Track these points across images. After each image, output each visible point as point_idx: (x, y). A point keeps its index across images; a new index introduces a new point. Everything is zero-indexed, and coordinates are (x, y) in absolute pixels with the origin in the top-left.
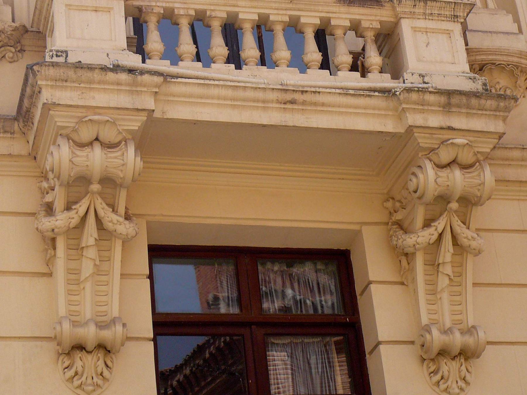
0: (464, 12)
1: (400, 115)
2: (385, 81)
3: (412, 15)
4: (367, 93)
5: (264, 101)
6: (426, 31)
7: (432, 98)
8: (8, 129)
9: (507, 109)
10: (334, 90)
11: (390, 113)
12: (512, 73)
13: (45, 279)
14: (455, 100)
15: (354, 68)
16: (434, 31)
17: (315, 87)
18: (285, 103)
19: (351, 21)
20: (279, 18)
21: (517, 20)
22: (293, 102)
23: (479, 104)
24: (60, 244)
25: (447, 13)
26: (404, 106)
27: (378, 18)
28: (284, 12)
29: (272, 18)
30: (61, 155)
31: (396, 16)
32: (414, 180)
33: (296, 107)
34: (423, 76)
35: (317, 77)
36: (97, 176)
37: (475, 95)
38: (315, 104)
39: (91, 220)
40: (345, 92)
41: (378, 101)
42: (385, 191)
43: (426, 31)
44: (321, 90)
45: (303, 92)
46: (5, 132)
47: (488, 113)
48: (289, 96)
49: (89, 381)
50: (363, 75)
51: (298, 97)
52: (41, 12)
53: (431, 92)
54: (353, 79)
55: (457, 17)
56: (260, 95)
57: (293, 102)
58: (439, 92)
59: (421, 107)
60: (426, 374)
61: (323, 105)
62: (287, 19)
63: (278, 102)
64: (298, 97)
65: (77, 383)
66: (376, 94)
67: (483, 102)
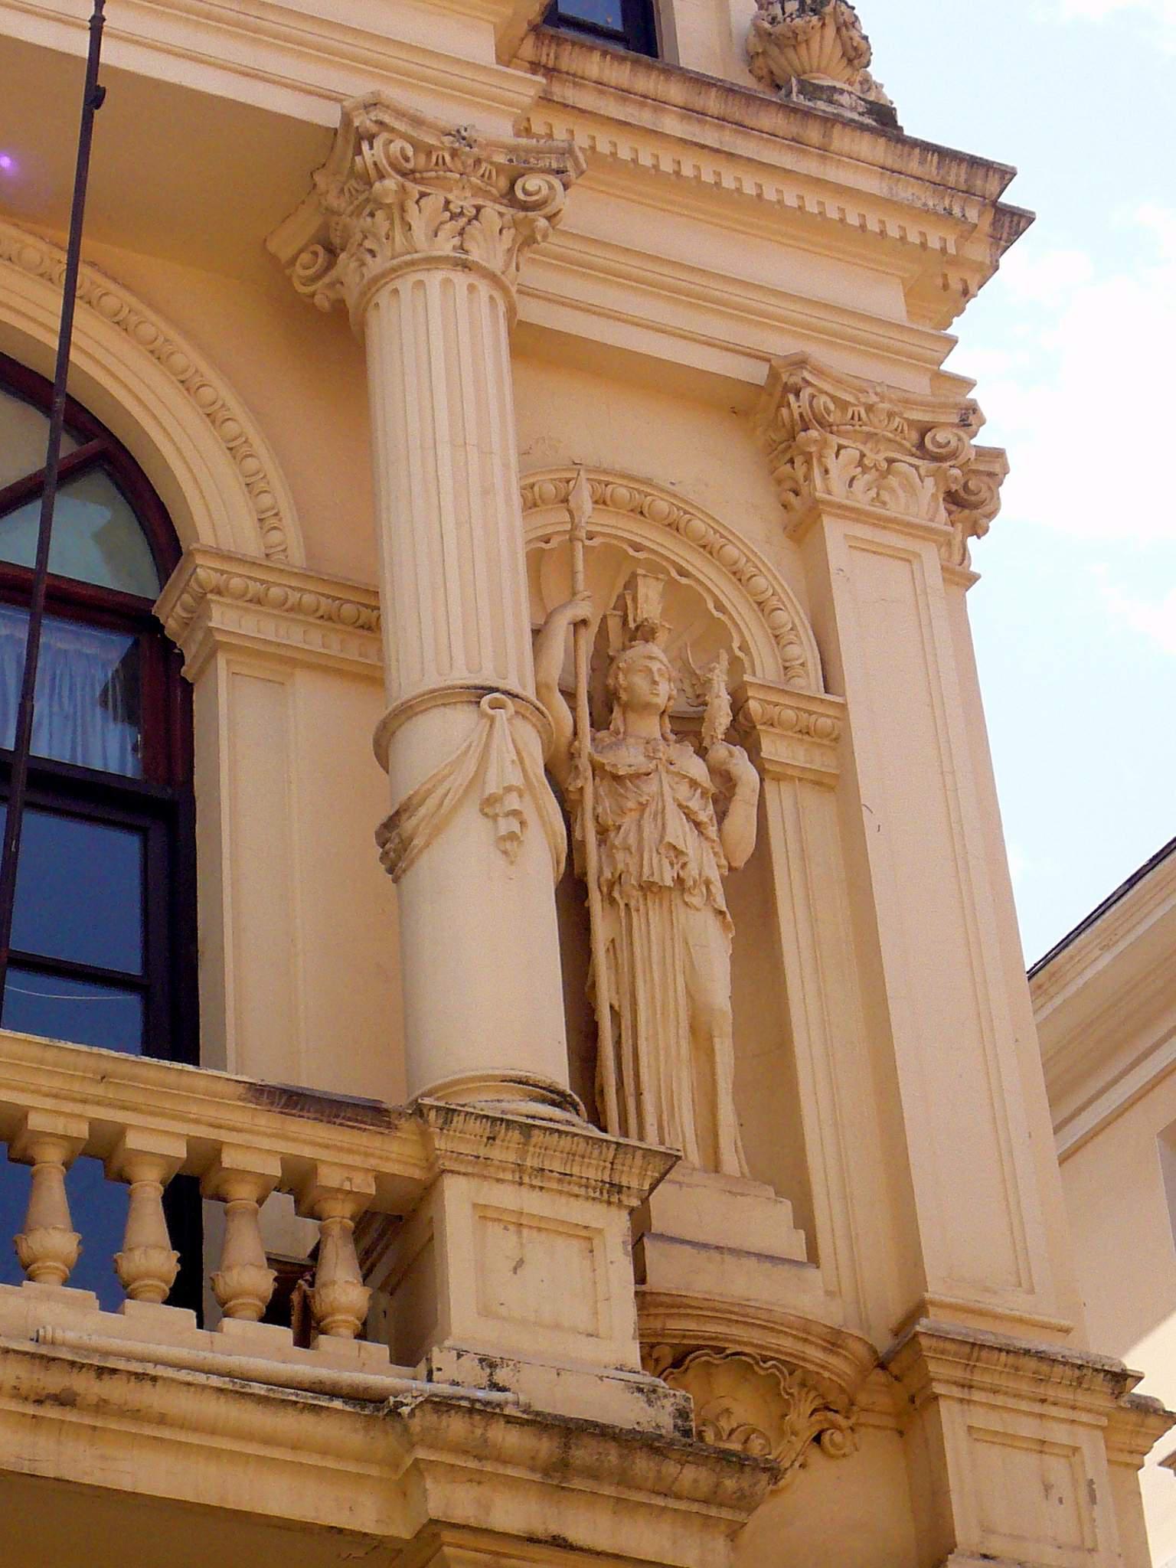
0: (642, 1176)
1: (406, 1480)
2: (373, 1367)
3: (481, 1168)
4: (309, 1398)
5: (806, 1340)
6: (519, 1223)
7: (510, 1439)
9: (746, 1502)
10: (201, 1378)
11: (374, 1471)
12: (773, 1389)
14: (583, 1453)
15: (275, 1312)
16: (543, 1226)
17: (142, 1360)
18: (39, 1402)
19: (286, 1162)
20: (59, 1126)
21: (804, 1220)
22: (65, 1400)
23: (659, 1478)
25: (591, 1174)
26: (421, 1454)
27: (372, 1162)
28: (78, 1108)
29: (35, 1122)
33: (71, 1416)
34: (493, 1366)
35: (154, 1328)
37: (650, 1443)
38: (136, 1415)
40: (239, 1386)
41: (339, 1429)
43: (519, 1223)
44: (160, 1371)
45: (101, 1371)
47: (683, 1506)
48: (54, 1381)
50: (304, 1340)
51: (84, 1385)
53: (509, 1420)
54: (267, 1350)
55: (619, 1189)
57: (65, 1400)
58: (538, 1422)
59: (472, 1464)
61: (162, 1420)
62: (82, 1130)
63: (17, 1394)
64: (84, 1385)
66: (337, 1404)
67: (670, 1468)
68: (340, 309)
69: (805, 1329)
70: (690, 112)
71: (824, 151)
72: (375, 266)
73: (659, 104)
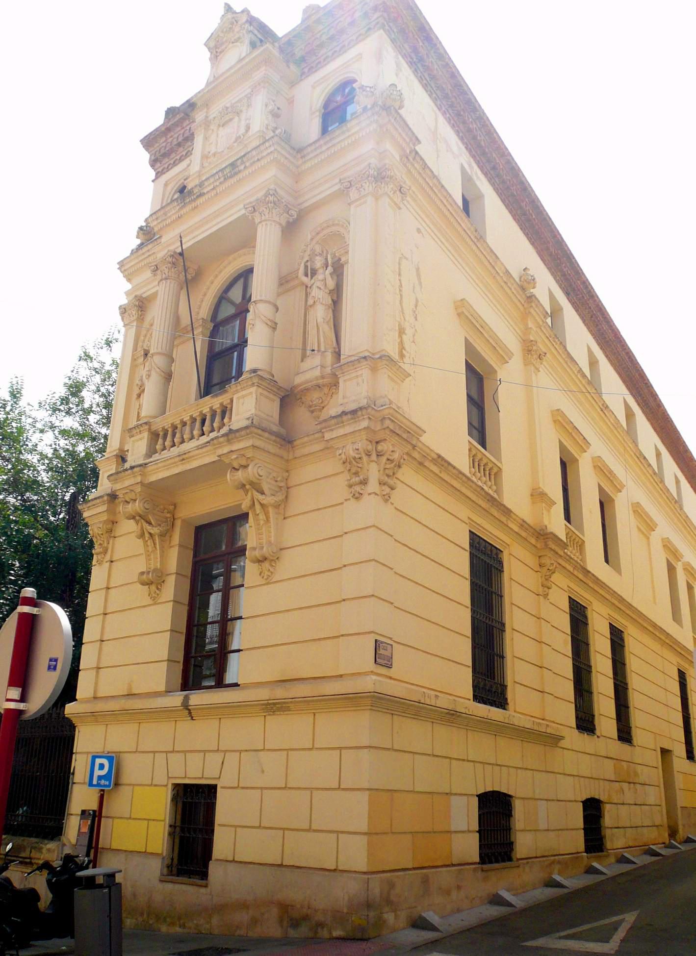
38: (191, 457)
48: (181, 458)
56: (173, 461)
57: (183, 460)
69: (317, 378)
70: (325, 144)
71: (348, 130)
73: (321, 146)
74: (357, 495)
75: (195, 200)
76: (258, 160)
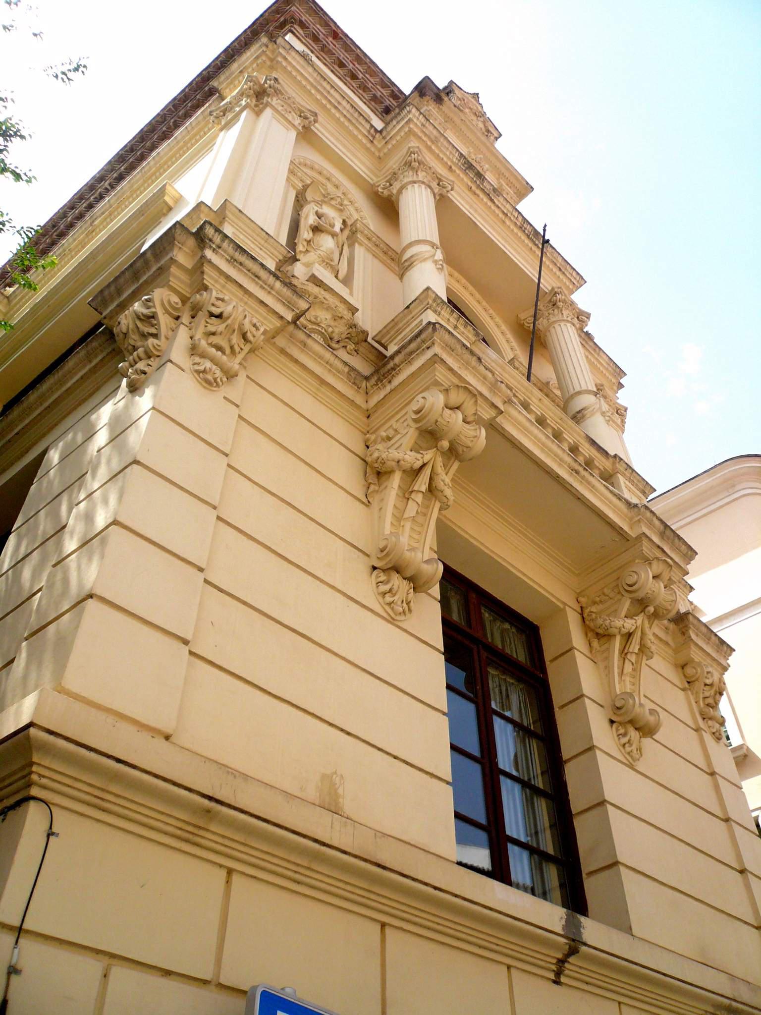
7: (657, 523)
8: (357, 382)
13: (362, 506)
24: (396, 480)
30: (435, 400)
31: (613, 470)
32: (636, 577)
36: (657, 603)
39: (427, 472)
42: (578, 591)
46: (354, 383)
49: (399, 603)
52: (396, 324)
60: (615, 735)
65: (388, 598)
68: (390, 196)
72: (552, 319)
74: (210, 377)
75: (478, 186)
76: (560, 270)
